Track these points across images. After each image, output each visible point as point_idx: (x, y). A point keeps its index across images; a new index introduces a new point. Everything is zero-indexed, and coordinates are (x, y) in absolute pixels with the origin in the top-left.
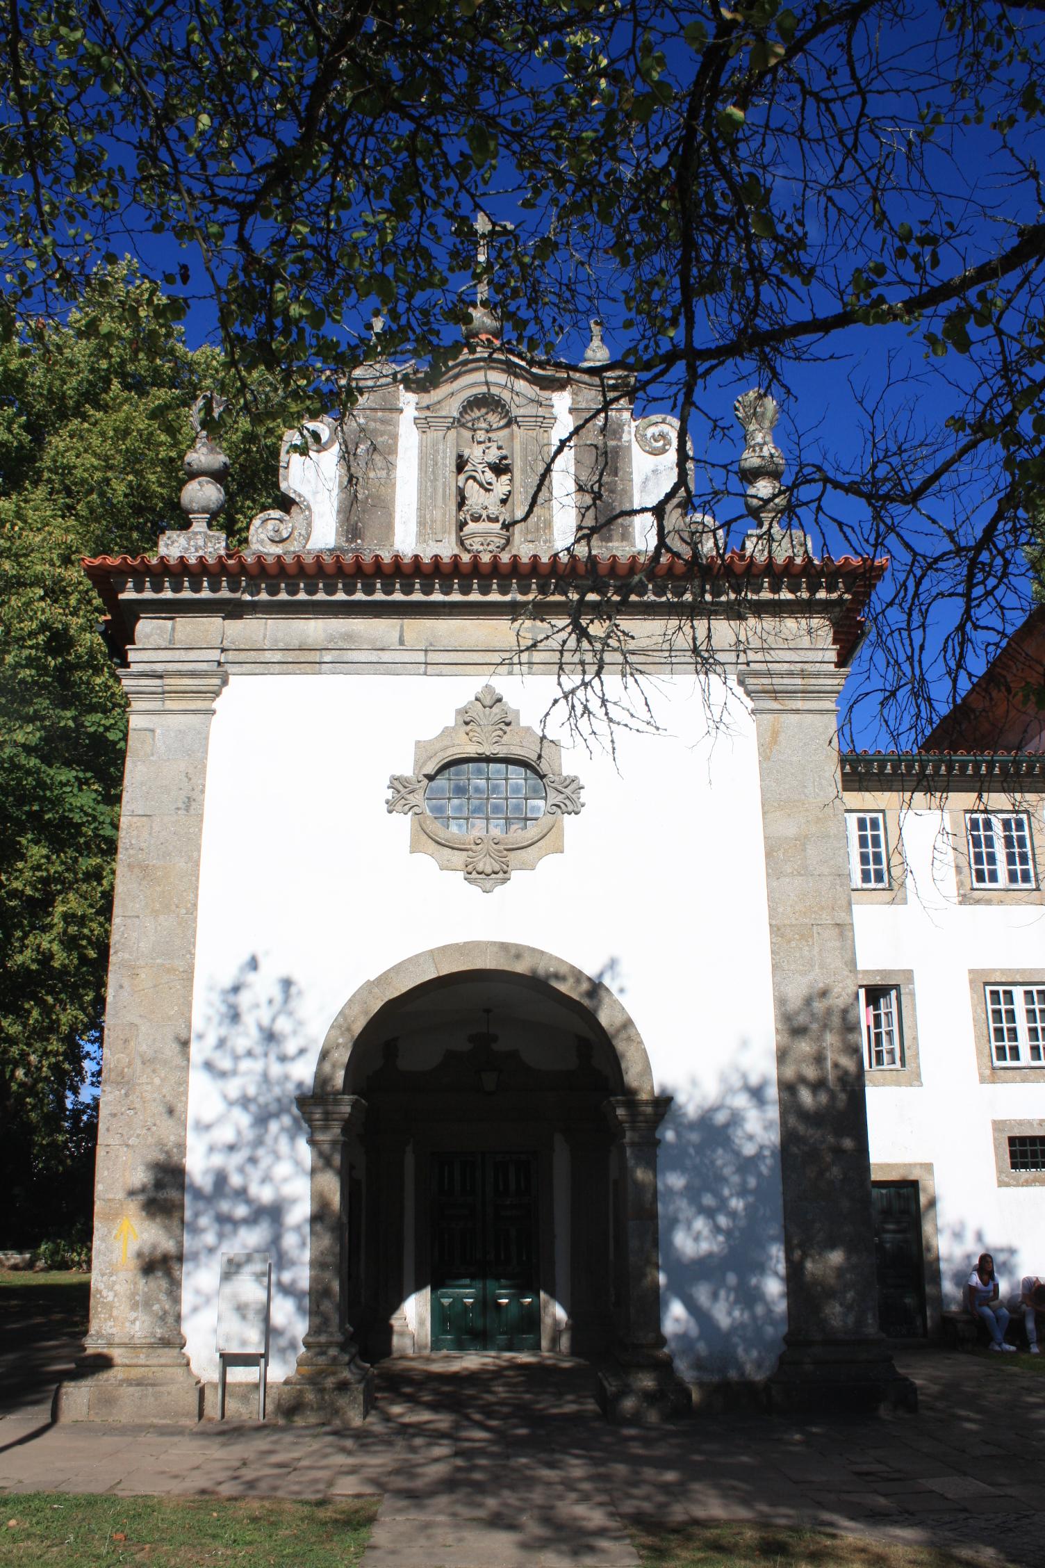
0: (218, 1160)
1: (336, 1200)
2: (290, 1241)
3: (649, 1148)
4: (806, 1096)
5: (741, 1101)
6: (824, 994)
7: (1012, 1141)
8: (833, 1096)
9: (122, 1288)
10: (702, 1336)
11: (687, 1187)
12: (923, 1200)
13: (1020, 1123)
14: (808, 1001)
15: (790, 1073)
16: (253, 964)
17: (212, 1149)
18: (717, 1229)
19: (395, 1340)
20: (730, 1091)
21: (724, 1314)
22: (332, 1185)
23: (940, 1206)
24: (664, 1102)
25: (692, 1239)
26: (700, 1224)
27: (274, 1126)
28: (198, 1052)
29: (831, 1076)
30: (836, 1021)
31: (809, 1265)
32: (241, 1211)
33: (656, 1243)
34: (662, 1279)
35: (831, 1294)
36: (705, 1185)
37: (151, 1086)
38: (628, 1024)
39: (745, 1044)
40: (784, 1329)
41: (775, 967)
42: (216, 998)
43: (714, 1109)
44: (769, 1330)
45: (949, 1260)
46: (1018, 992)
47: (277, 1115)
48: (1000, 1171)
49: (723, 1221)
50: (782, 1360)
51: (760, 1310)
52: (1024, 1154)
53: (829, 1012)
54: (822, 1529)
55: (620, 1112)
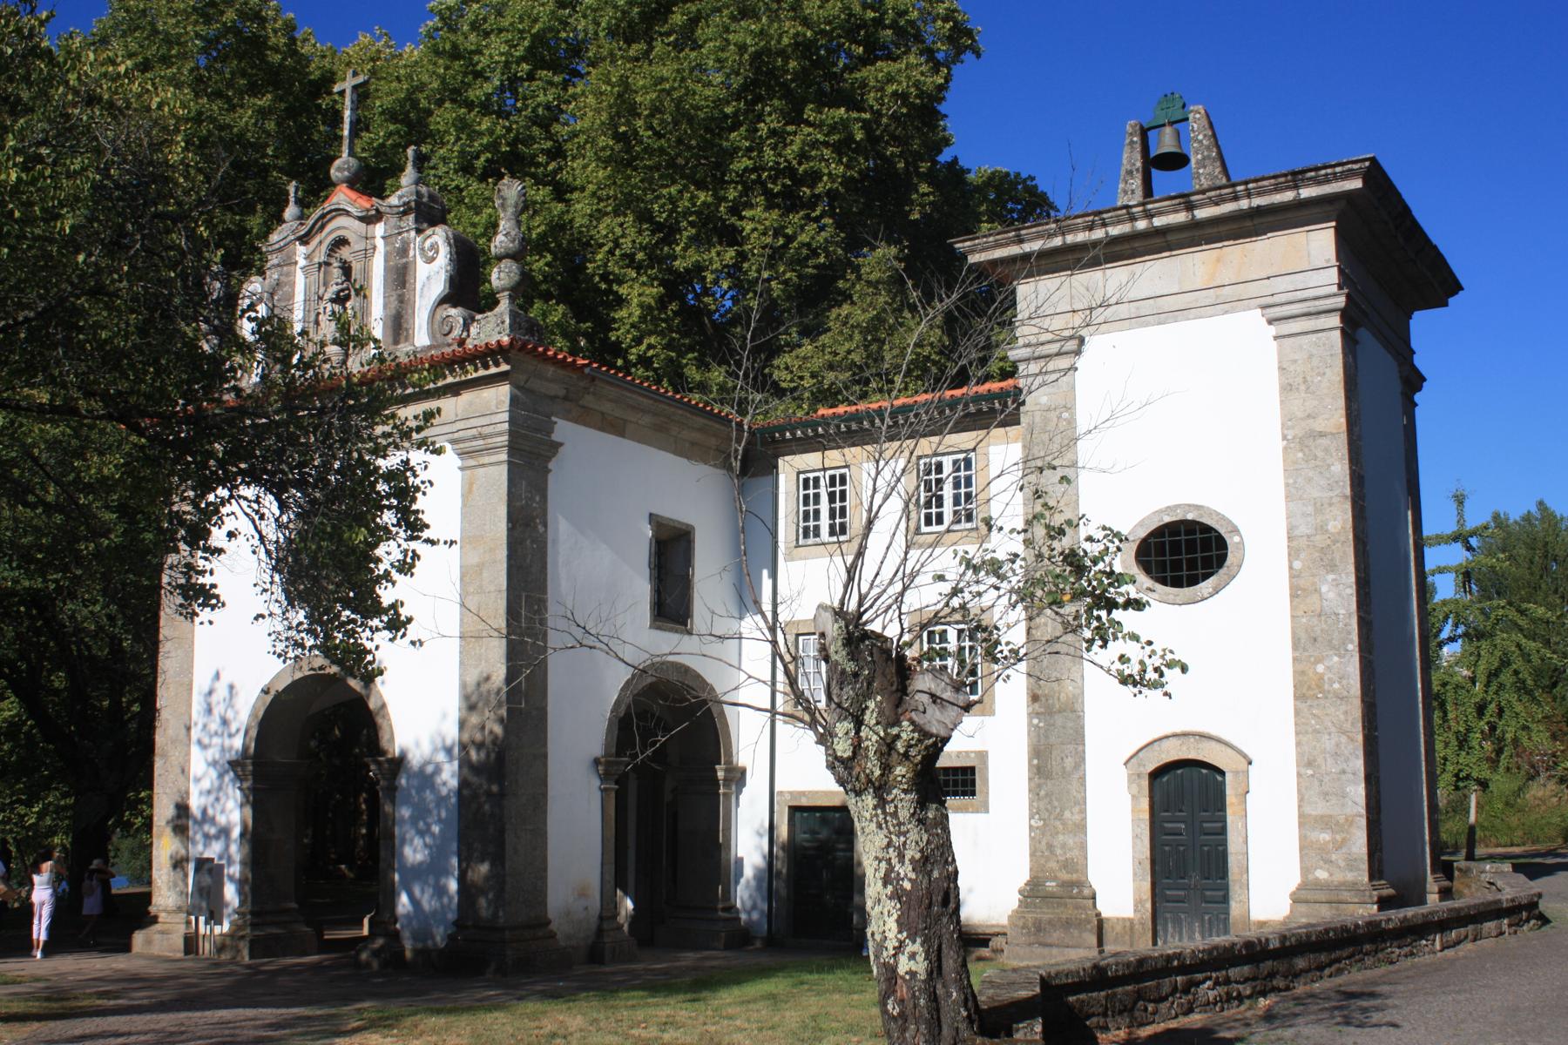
0: (203, 800)
4: (474, 755)
5: (441, 757)
6: (488, 679)
8: (488, 755)
9: (165, 878)
11: (411, 817)
14: (479, 685)
16: (217, 676)
17: (201, 793)
20: (435, 750)
21: (428, 902)
22: (248, 811)
24: (399, 762)
25: (414, 852)
26: (418, 841)
27: (227, 779)
28: (195, 733)
29: (488, 740)
32: (213, 831)
37: (175, 755)
38: (384, 706)
39: (444, 716)
41: (461, 663)
42: (202, 699)
43: (428, 763)
49: (428, 840)
51: (445, 900)
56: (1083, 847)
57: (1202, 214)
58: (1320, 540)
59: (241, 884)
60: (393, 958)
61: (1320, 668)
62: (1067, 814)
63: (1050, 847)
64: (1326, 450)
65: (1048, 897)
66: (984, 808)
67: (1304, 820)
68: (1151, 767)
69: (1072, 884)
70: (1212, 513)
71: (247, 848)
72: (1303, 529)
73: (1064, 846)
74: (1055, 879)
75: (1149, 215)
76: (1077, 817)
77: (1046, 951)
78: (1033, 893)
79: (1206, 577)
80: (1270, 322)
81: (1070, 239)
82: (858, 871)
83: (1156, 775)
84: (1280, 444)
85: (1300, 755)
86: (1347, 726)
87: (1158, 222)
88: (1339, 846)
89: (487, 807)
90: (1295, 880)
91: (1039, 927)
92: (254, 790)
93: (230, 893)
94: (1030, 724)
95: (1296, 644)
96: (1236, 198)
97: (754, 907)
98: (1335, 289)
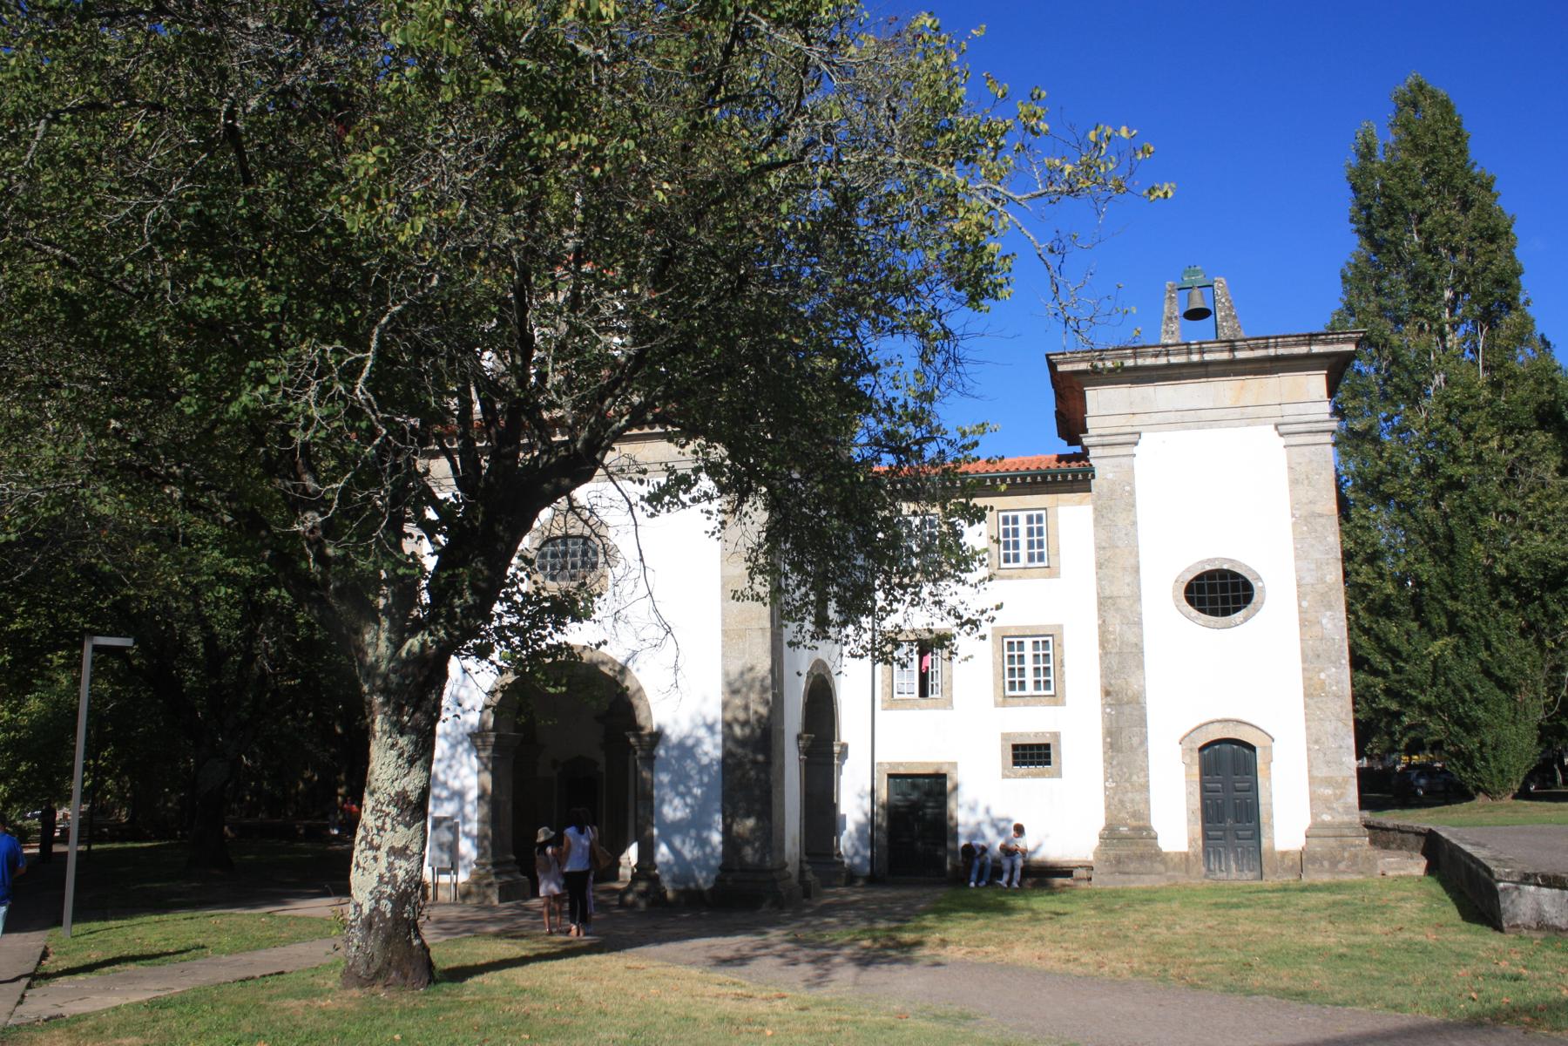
1: (489, 787)
2: (469, 809)
3: (650, 759)
4: (738, 730)
6: (751, 669)
7: (1015, 747)
8: (753, 730)
10: (676, 863)
12: (949, 785)
13: (1021, 735)
14: (742, 674)
15: (729, 716)
18: (686, 805)
19: (621, 870)
20: (696, 726)
21: (689, 852)
22: (487, 778)
23: (961, 789)
24: (658, 736)
25: (673, 810)
26: (677, 801)
27: (460, 749)
29: (753, 718)
30: (757, 685)
31: (735, 827)
32: (445, 794)
33: (652, 813)
34: (655, 832)
35: (748, 842)
36: (680, 781)
38: (640, 689)
39: (705, 699)
40: (720, 862)
41: (723, 655)
43: (687, 737)
44: (713, 862)
45: (966, 825)
46: (1028, 643)
47: (460, 743)
48: (1004, 768)
49: (689, 800)
50: (718, 879)
51: (708, 850)
52: (1024, 756)
53: (753, 680)
54: (504, 926)
55: (632, 740)
56: (1147, 802)
57: (1240, 355)
58: (1321, 588)
59: (480, 841)
60: (654, 895)
61: (1323, 676)
62: (1135, 778)
63: (1121, 802)
64: (1323, 526)
65: (1122, 838)
66: (1059, 774)
67: (1312, 780)
68: (1201, 744)
69: (1141, 829)
70: (1241, 565)
71: (486, 809)
72: (1308, 579)
73: (1132, 801)
74: (1126, 825)
75: (1202, 352)
76: (1142, 780)
77: (1125, 877)
78: (1110, 835)
79: (1236, 610)
80: (1281, 435)
81: (1140, 362)
82: (951, 824)
83: (1201, 749)
84: (1289, 521)
85: (1309, 735)
86: (1343, 716)
87: (1207, 357)
88: (1338, 798)
89: (752, 773)
90: (1307, 822)
91: (1119, 861)
92: (494, 759)
93: (467, 848)
94: (1104, 712)
95: (1305, 659)
96: (1267, 347)
97: (856, 853)
98: (1327, 417)
